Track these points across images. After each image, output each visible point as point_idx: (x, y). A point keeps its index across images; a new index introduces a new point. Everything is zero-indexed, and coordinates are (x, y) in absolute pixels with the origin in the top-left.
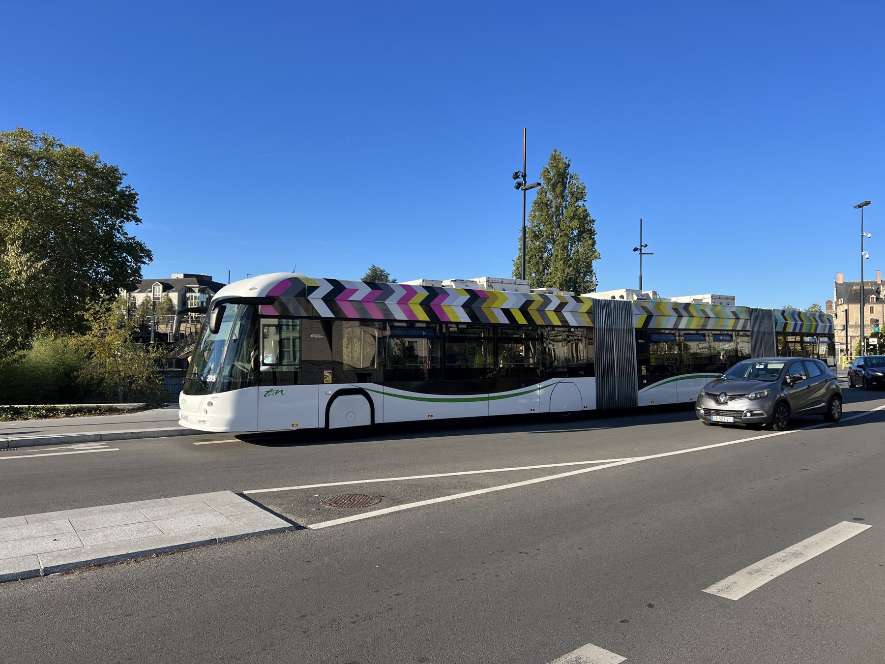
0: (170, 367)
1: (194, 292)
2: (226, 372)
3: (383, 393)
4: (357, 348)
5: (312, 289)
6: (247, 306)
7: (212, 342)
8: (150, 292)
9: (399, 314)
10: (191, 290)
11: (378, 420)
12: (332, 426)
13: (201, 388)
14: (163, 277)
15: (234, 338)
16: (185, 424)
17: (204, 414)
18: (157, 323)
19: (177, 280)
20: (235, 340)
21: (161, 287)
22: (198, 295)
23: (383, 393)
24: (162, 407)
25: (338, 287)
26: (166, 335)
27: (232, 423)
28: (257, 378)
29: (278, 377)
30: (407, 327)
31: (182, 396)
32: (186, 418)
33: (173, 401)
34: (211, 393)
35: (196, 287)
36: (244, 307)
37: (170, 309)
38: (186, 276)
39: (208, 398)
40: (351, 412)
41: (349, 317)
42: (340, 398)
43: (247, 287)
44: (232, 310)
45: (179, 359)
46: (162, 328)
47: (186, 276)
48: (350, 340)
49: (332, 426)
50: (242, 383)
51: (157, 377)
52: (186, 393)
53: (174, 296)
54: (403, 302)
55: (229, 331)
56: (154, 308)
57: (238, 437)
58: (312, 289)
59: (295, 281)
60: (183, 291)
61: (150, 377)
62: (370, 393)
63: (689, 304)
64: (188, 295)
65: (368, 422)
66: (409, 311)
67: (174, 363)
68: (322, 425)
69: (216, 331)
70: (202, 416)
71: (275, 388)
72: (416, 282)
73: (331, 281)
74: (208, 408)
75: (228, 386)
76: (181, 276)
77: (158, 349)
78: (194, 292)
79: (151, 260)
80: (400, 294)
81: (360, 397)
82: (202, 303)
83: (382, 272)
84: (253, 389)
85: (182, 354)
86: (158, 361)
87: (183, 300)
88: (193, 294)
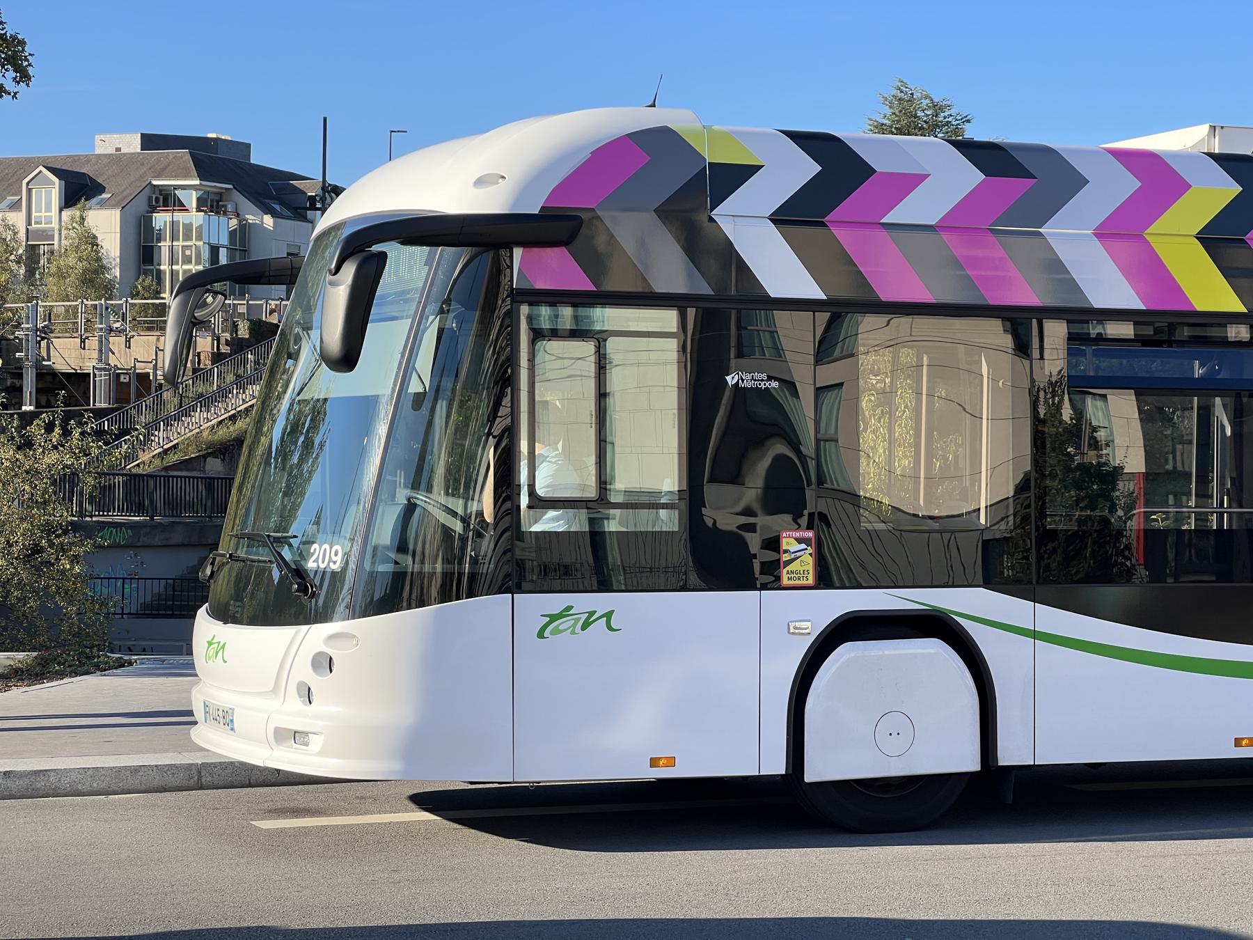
0: (103, 507)
1: (181, 207)
2: (385, 534)
3: (1035, 635)
4: (928, 434)
5: (731, 177)
6: (464, 254)
7: (318, 410)
8: (15, 206)
9: (1109, 287)
10: (167, 200)
11: (1011, 753)
12: (812, 774)
13: (290, 598)
14: (64, 149)
15: (415, 387)
16: (214, 744)
17: (296, 703)
18: (44, 334)
19: (118, 159)
20: (419, 399)
21: (53, 190)
22: (195, 218)
23: (1035, 635)
24: (100, 668)
25: (838, 172)
26: (80, 380)
27: (415, 743)
28: (514, 563)
29: (614, 555)
30: (1140, 340)
31: (205, 626)
32: (226, 719)
33: (175, 651)
34: (323, 616)
35: (189, 187)
36: (453, 258)
37: (93, 277)
38: (149, 141)
39: (315, 636)
40: (896, 715)
41: (886, 295)
42: (846, 653)
43: (461, 177)
44: (408, 268)
45: (133, 478)
46: (66, 355)
47: (149, 141)
48: (887, 396)
49: (812, 774)
50: (447, 576)
51: (62, 549)
52: (223, 615)
53: (106, 225)
54: (1123, 231)
55: (400, 351)
56: (31, 272)
57: (424, 801)
58: (731, 177)
59: (662, 141)
60: (141, 205)
61: (37, 550)
62: (975, 631)
63: (37, 374)
64: (161, 219)
65: (967, 760)
66: (1149, 269)
67: (119, 493)
68: (776, 765)
69: (347, 359)
70: (292, 713)
71: (584, 602)
72: (1180, 141)
73: (809, 142)
74: (314, 680)
75: (392, 594)
76: (132, 144)
77: (66, 433)
78: (181, 207)
79: (23, 76)
80: (1109, 190)
81: (933, 652)
82: (214, 250)
83: (938, 108)
84: (490, 609)
85: (144, 457)
86: (66, 482)
87: (144, 250)
88: (180, 217)
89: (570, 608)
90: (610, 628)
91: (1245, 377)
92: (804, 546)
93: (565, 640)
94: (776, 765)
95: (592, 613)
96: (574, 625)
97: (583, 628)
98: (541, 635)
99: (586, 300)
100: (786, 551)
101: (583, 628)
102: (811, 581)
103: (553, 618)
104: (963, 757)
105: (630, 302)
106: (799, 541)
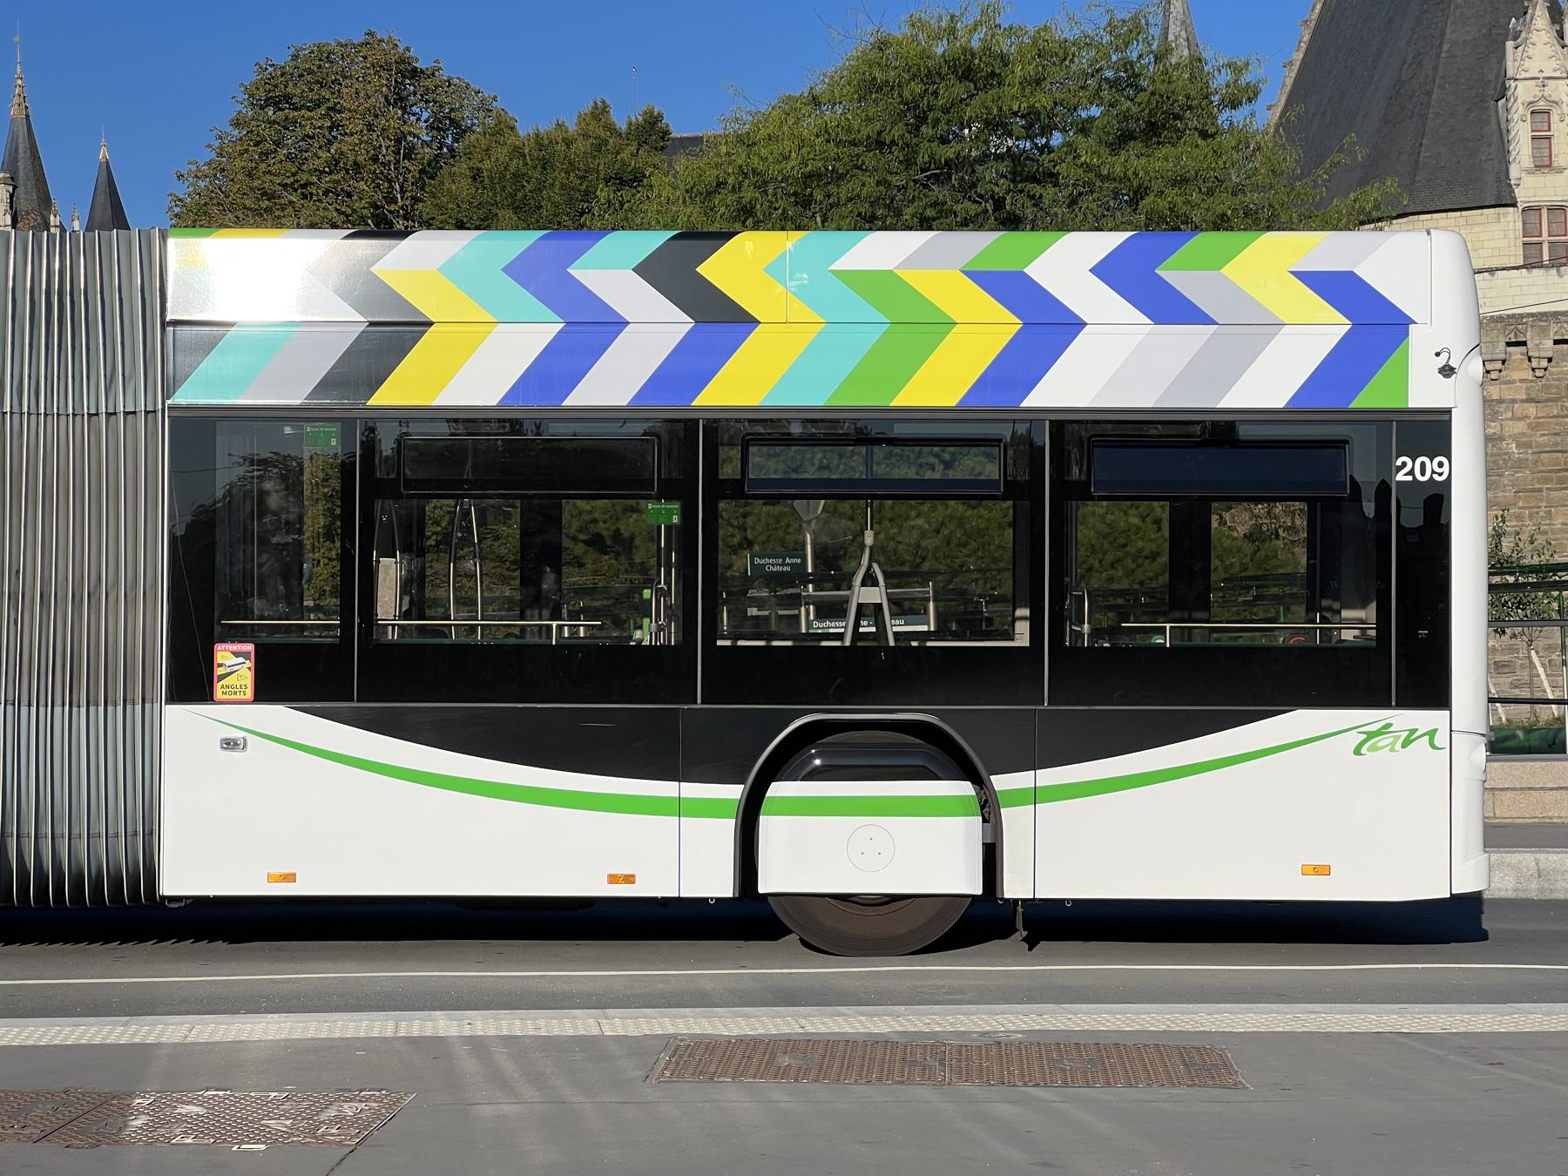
11: (1015, 887)
68: (972, 885)
89: (1390, 725)
90: (1433, 746)
91: (1412, 404)
92: (242, 660)
93: (1383, 757)
94: (972, 885)
95: (1413, 731)
96: (1393, 743)
97: (1404, 745)
98: (1357, 751)
99: (960, 416)
100: (220, 665)
101: (1404, 745)
102: (249, 695)
103: (1371, 735)
104: (719, 884)
105: (596, 415)
106: (236, 654)
